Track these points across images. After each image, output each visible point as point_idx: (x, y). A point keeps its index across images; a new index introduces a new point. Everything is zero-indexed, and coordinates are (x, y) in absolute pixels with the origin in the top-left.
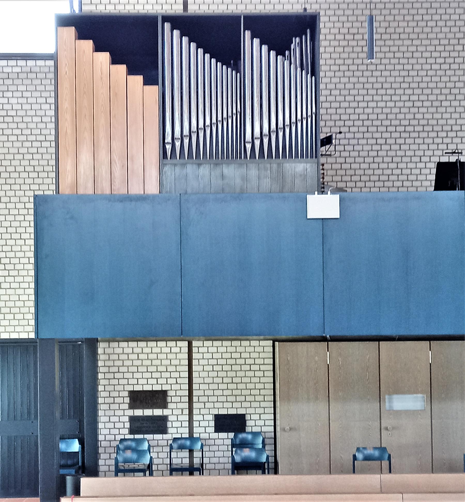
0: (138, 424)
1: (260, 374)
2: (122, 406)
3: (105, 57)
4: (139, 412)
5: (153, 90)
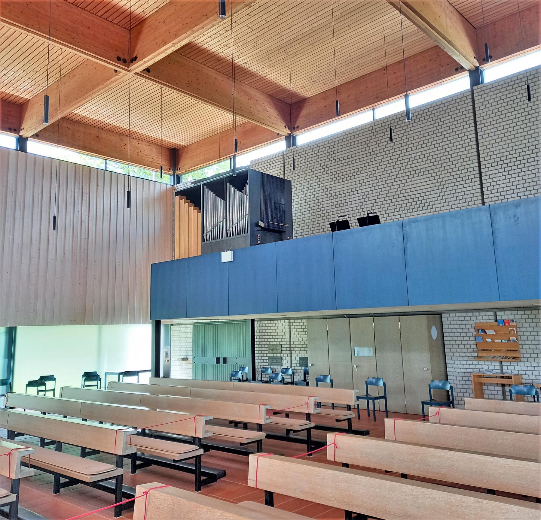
4: (279, 355)
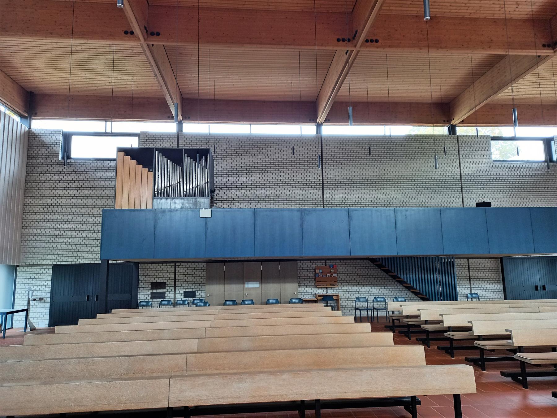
0: (154, 295)
2: (148, 289)
3: (134, 162)
4: (154, 291)
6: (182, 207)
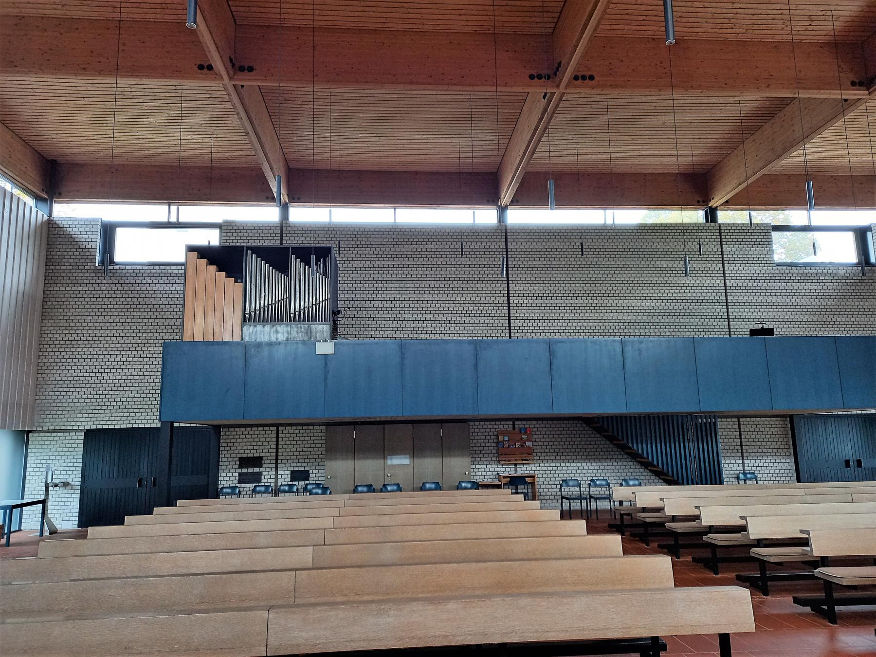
1: (319, 445)
4: (244, 470)
5: (240, 286)
6: (287, 339)
